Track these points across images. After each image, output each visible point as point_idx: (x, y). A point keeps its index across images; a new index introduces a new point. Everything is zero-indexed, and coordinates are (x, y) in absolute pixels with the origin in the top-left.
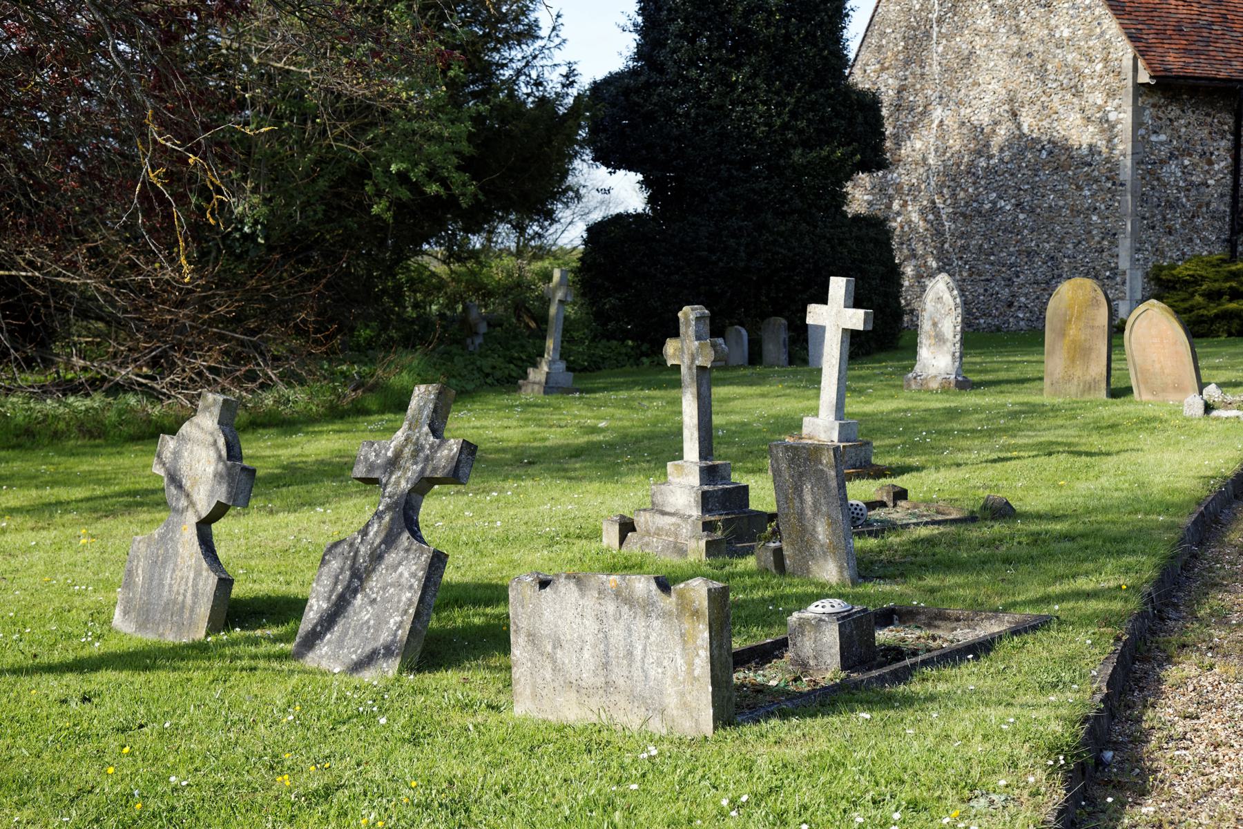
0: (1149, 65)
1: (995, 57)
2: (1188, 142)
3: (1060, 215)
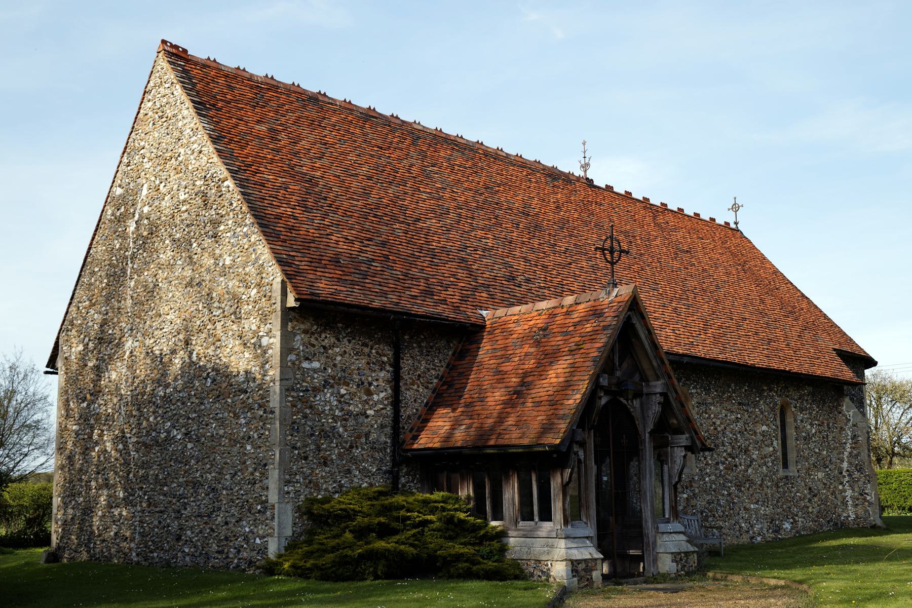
0: (295, 287)
1: (174, 289)
2: (344, 371)
3: (220, 445)
